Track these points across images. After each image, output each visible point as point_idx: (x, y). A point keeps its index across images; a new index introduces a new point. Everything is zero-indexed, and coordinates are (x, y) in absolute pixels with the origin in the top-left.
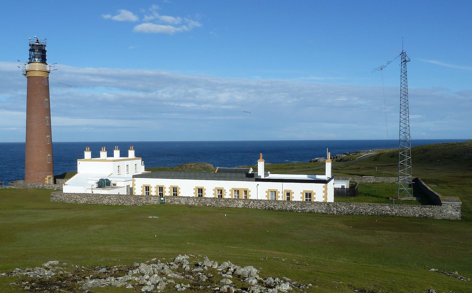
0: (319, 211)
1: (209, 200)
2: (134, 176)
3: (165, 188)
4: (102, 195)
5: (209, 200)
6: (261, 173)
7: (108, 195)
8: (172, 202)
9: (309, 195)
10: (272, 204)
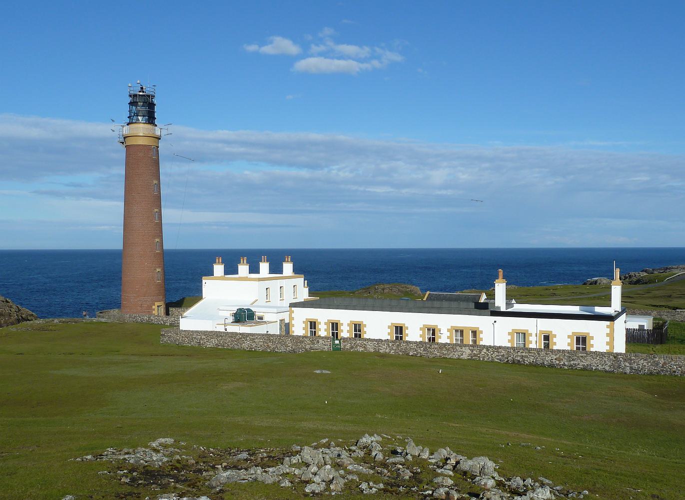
0: (600, 367)
1: (414, 346)
2: (293, 305)
4: (240, 334)
5: (414, 346)
6: (500, 301)
7: (251, 334)
8: (352, 348)
9: (582, 340)
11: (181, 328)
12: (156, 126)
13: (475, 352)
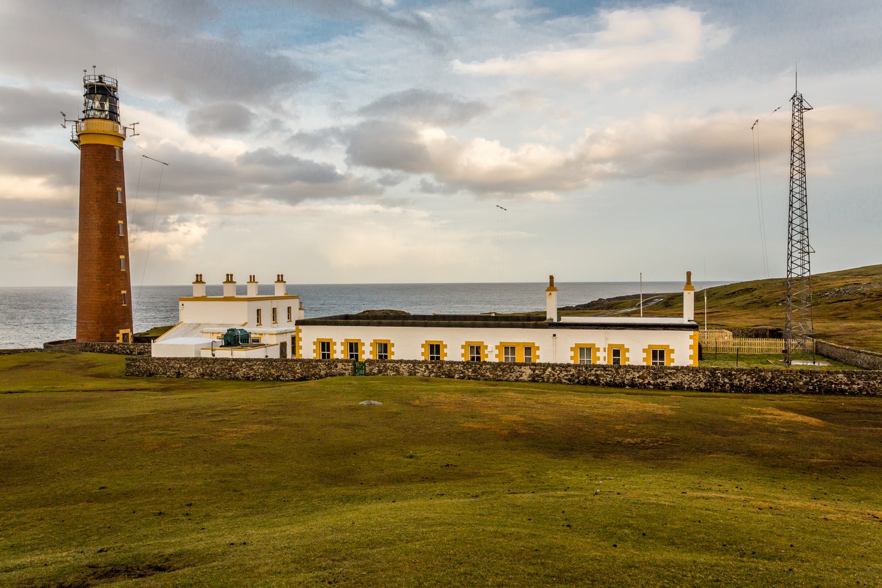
1: (460, 367)
2: (299, 323)
3: (335, 344)
4: (234, 360)
5: (460, 367)
10: (593, 372)
11: (153, 356)
12: (119, 123)
13: (537, 372)
